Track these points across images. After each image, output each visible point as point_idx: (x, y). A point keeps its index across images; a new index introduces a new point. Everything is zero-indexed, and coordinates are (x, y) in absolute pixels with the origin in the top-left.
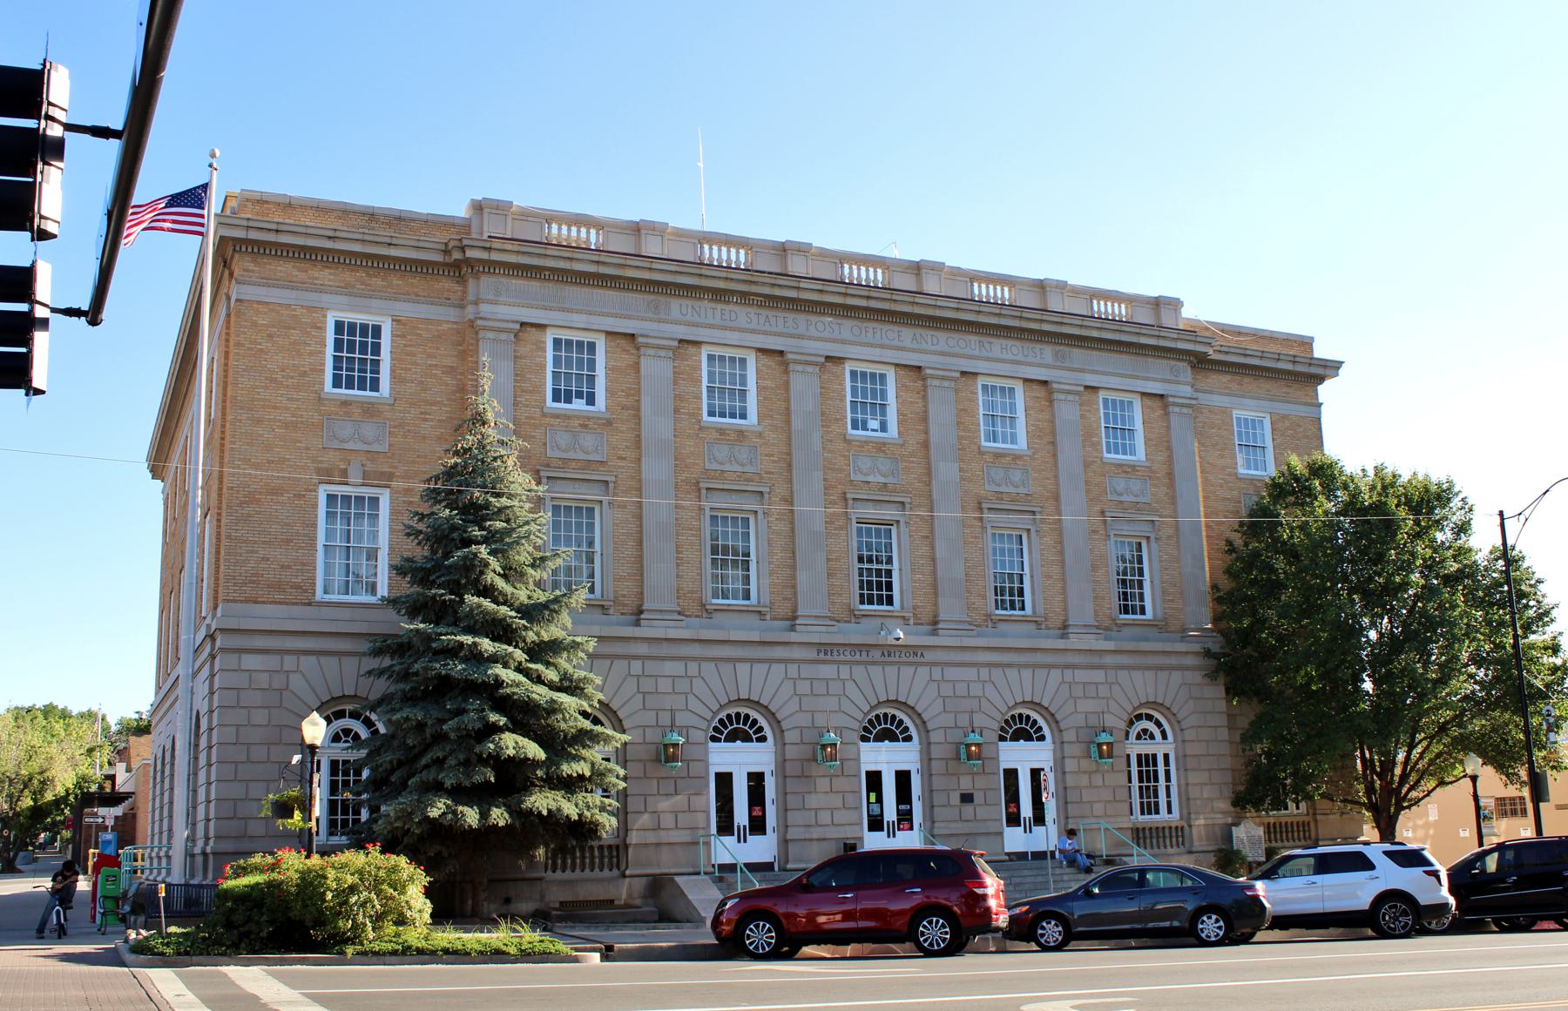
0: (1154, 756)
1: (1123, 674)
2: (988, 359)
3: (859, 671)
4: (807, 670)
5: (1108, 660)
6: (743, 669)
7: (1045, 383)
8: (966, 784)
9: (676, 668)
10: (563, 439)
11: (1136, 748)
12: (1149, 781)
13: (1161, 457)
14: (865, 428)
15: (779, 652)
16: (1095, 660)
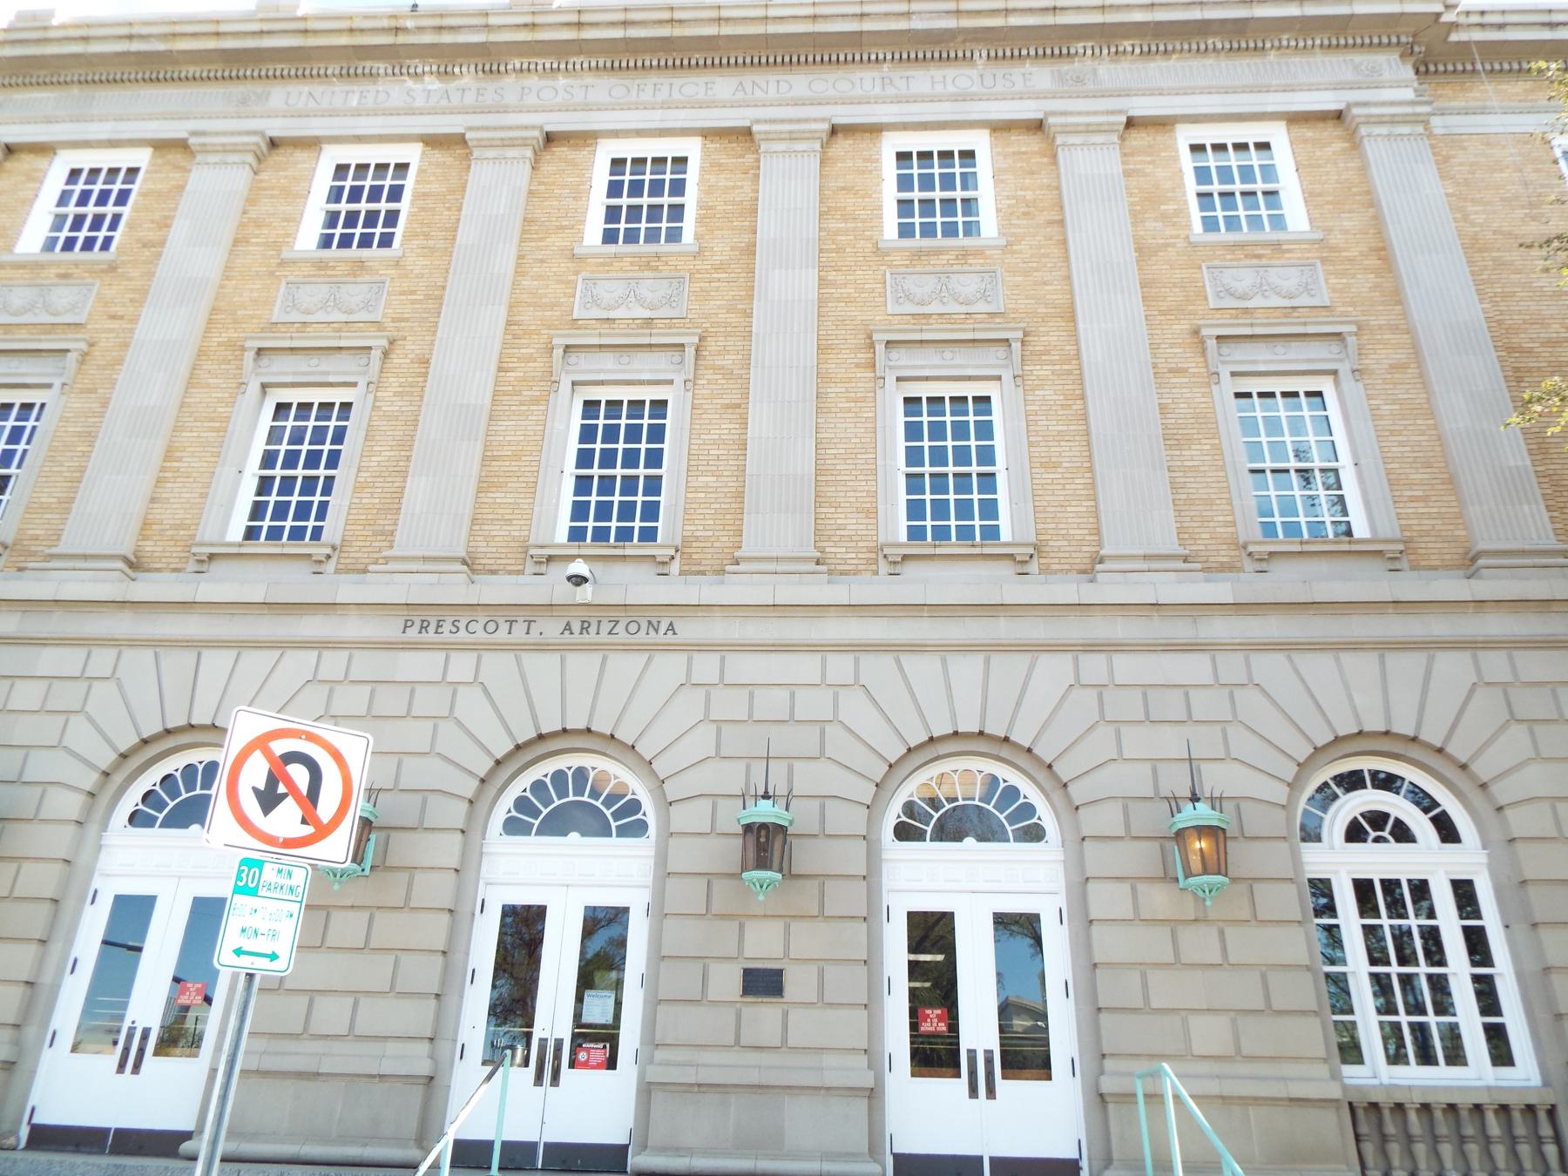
3: (498, 667)
4: (367, 665)
5: (1219, 628)
8: (763, 946)
9: (66, 660)
13: (1353, 221)
15: (312, 627)
16: (1181, 630)
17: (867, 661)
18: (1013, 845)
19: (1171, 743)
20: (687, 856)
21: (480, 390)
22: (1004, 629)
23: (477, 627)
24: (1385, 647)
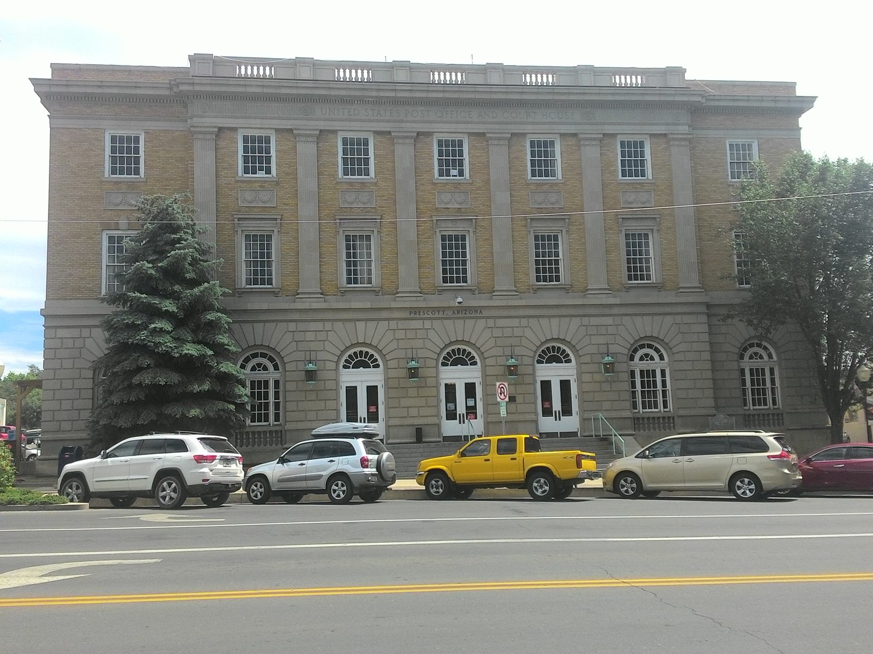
0: (654, 371)
1: (626, 319)
2: (533, 123)
3: (437, 324)
4: (402, 324)
5: (615, 311)
6: (360, 325)
7: (575, 135)
9: (319, 326)
10: (249, 196)
11: (638, 365)
12: (649, 387)
14: (448, 175)
15: (385, 314)
16: (607, 311)
17: (531, 320)
18: (372, 369)
19: (602, 340)
20: (392, 373)
21: (413, 236)
22: (564, 312)
23: (430, 313)
24: (550, 317)
